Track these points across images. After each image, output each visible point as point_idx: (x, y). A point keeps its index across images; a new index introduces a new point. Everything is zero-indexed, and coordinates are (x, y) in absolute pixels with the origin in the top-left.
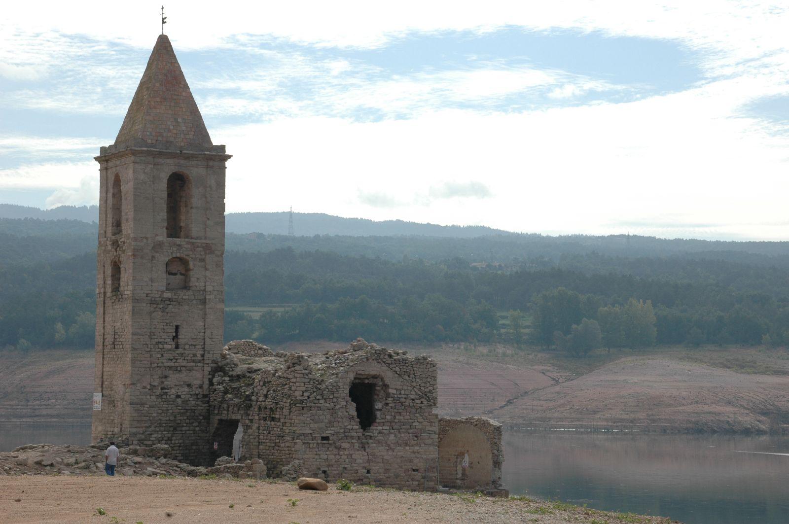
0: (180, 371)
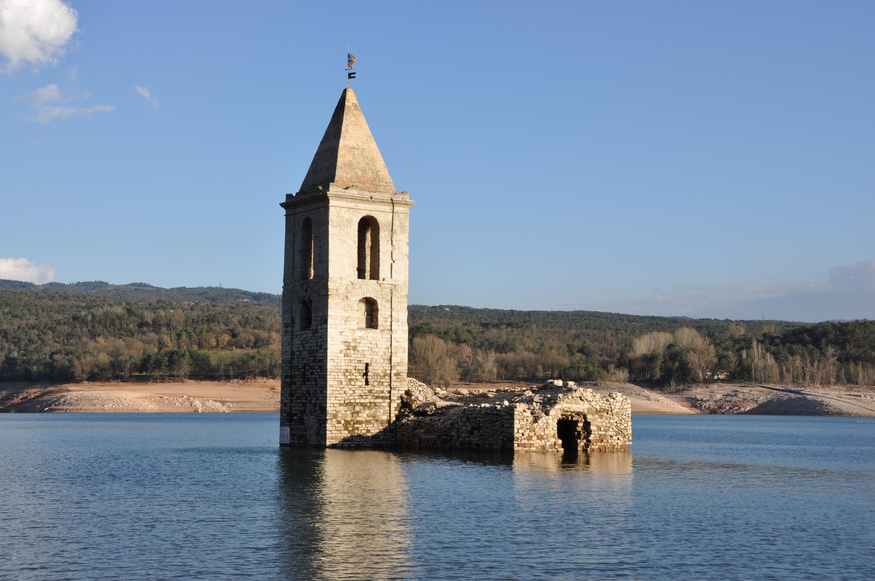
0: (369, 407)
